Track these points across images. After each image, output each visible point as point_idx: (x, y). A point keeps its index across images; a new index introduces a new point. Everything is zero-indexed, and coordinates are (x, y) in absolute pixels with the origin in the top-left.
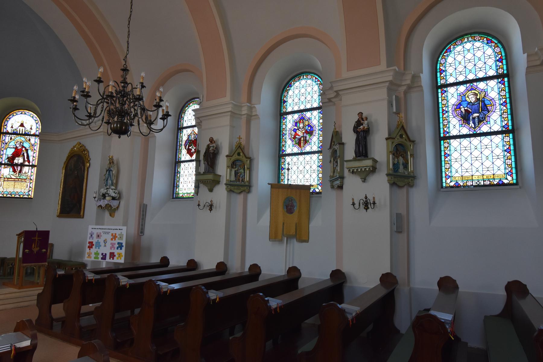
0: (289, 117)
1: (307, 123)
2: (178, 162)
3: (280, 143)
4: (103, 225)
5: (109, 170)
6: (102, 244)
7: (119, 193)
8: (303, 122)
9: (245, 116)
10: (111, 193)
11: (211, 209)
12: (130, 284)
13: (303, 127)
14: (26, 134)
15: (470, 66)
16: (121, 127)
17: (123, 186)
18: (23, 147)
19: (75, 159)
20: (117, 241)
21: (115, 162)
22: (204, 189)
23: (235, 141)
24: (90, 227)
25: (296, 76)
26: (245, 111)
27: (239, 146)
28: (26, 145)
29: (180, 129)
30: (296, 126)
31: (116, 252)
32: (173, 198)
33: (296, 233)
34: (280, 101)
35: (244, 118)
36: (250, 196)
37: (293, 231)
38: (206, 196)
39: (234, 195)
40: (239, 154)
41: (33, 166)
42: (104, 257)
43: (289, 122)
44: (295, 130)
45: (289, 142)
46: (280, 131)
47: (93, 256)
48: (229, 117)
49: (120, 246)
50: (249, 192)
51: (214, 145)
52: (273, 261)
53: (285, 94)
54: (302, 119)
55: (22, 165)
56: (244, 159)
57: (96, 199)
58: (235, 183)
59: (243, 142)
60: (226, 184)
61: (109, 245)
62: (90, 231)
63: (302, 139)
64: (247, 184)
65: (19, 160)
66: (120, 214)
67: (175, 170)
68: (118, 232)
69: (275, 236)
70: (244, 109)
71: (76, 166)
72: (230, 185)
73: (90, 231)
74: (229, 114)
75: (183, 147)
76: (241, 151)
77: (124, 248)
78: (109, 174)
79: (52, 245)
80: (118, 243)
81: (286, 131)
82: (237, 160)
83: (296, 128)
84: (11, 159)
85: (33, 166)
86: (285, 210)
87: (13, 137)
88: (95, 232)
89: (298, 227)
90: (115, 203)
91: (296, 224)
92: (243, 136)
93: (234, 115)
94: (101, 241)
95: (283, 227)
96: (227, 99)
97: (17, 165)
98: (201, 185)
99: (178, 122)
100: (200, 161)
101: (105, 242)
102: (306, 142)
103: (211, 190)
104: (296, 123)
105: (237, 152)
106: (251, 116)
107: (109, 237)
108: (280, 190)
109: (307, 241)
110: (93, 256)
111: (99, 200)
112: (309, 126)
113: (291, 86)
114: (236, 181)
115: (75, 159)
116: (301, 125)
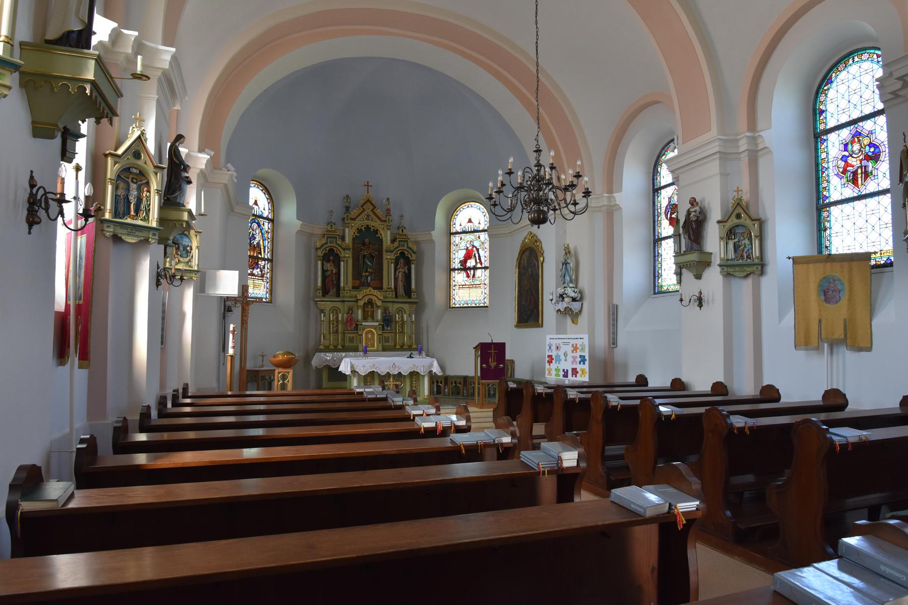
0: (832, 137)
1: (866, 141)
2: (657, 241)
3: (818, 184)
4: (565, 333)
5: (565, 263)
6: (562, 357)
7: (581, 292)
8: (859, 141)
9: (746, 153)
10: (570, 292)
11: (700, 305)
12: (580, 399)
13: (860, 150)
14: (475, 231)
15: (855, 99)
16: (539, 217)
17: (584, 283)
18: (473, 246)
19: (527, 253)
20: (579, 353)
21: (572, 251)
22: (687, 275)
23: (732, 196)
24: (548, 337)
25: (839, 62)
26: (743, 145)
27: (738, 204)
28: (477, 244)
29: (656, 190)
30: (846, 150)
31: (579, 367)
32: (655, 293)
33: (845, 335)
34: (816, 112)
35: (745, 158)
36: (765, 281)
37: (839, 333)
38: (692, 286)
39: (735, 282)
40: (738, 216)
41: (486, 268)
42: (566, 375)
43: (833, 145)
44: (845, 158)
45: (835, 181)
46: (817, 165)
47: (553, 372)
48: (717, 162)
49: (583, 360)
50: (762, 273)
51: (697, 208)
52: (800, 379)
53: (822, 98)
54: (858, 134)
55: (475, 268)
56: (748, 222)
57: (554, 302)
58: (736, 262)
59: (746, 197)
60: (720, 265)
61: (570, 359)
62: (548, 343)
63: (859, 171)
64: (756, 261)
65: (471, 263)
66: (583, 319)
67: (654, 252)
68: (579, 342)
69: (805, 340)
70: (740, 143)
71: (529, 263)
72: (727, 266)
73: (548, 343)
74: (718, 156)
75: (663, 216)
76: (741, 211)
77: (587, 363)
78: (566, 269)
79: (512, 362)
80: (581, 356)
81: (828, 162)
82: (737, 226)
83: (846, 153)
84: (464, 262)
85: (486, 268)
86: (823, 298)
87: (462, 235)
88: (554, 342)
89: (849, 326)
90: (576, 306)
91: (845, 320)
92: (745, 187)
93: (724, 157)
94: (561, 353)
95: (820, 326)
96: (713, 133)
97: (470, 269)
98: (684, 271)
99: (653, 180)
100: (680, 235)
101: (565, 354)
102: (867, 175)
103: (698, 277)
104: (846, 146)
105: (734, 214)
106: (757, 151)
107: (569, 349)
108: (811, 265)
109: (869, 349)
110: (553, 372)
111: (557, 302)
112: (871, 145)
113: (832, 82)
114: (736, 258)
115: (527, 253)
116: (856, 147)
